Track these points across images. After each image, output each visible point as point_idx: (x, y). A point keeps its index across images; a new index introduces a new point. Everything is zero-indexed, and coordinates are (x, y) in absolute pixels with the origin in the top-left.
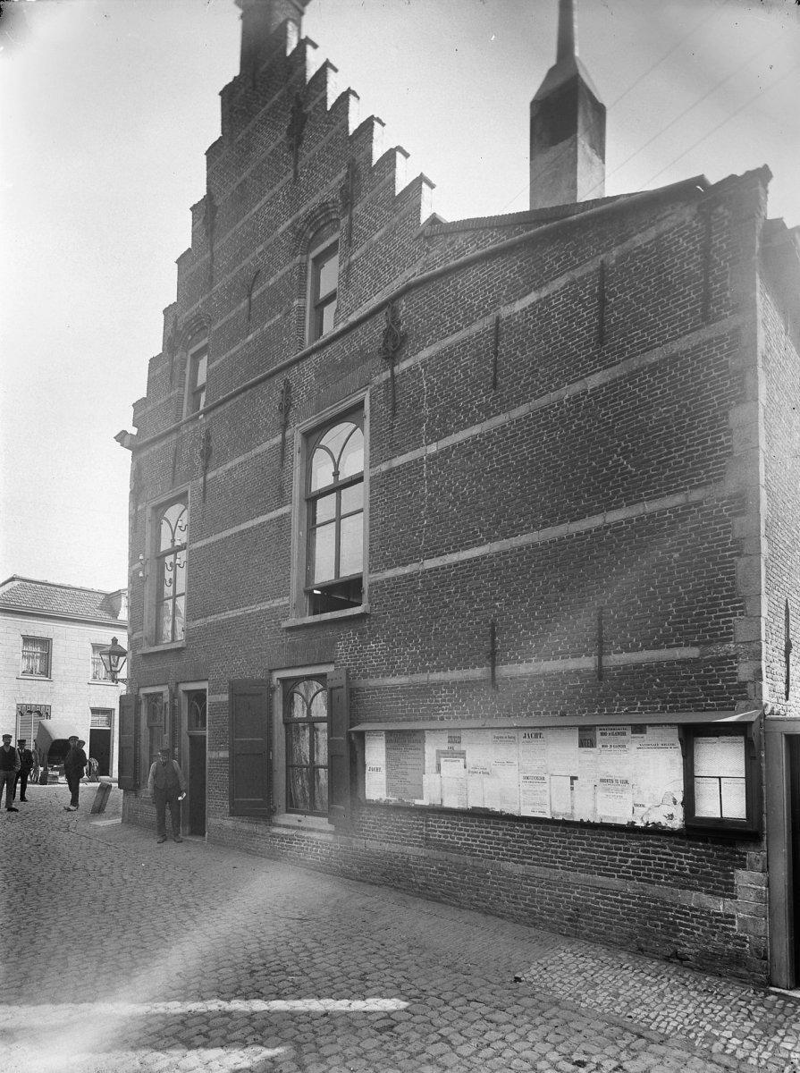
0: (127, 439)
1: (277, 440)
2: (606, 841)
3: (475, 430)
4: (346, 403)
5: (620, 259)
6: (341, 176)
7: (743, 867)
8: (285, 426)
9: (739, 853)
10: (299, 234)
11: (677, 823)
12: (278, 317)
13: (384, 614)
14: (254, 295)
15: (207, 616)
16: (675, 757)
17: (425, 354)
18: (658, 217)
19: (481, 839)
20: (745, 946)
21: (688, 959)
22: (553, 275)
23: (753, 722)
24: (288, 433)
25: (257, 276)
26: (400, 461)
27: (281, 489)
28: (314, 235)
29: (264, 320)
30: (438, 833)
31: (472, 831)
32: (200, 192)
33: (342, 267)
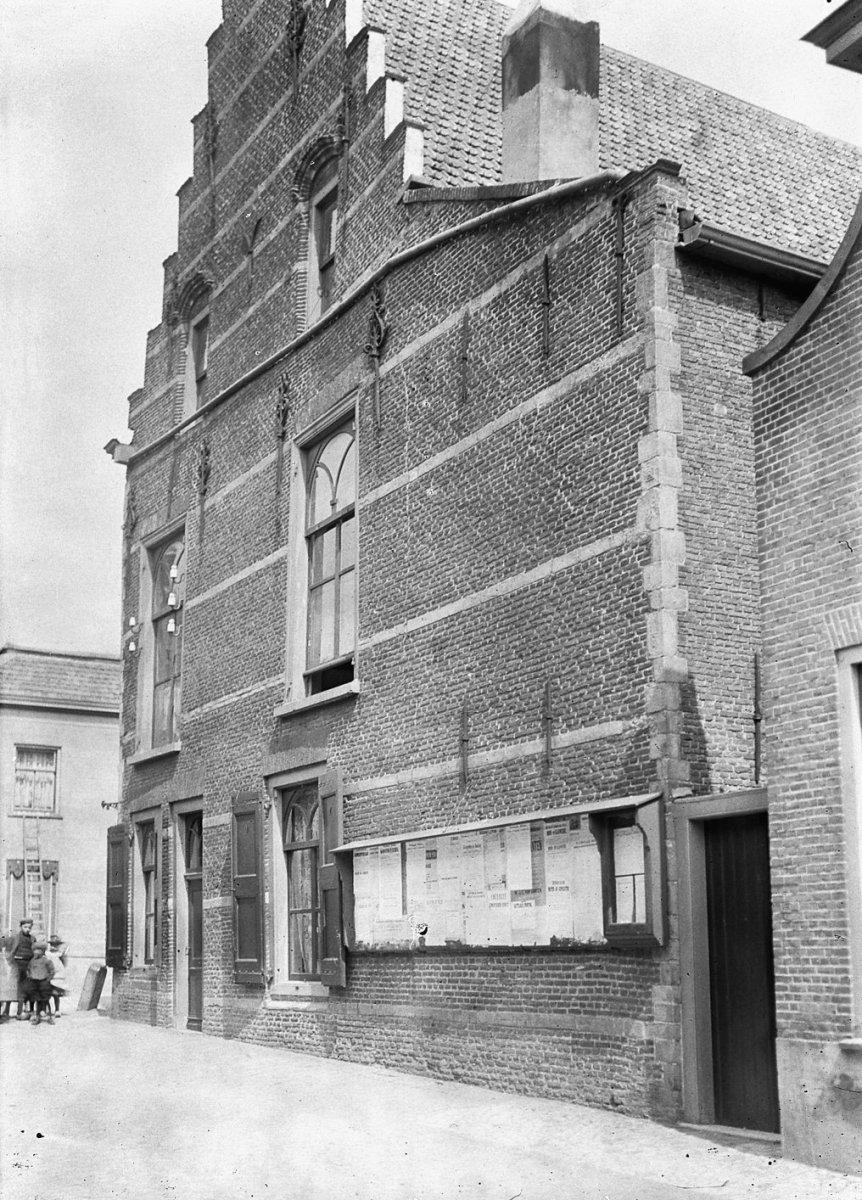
0: (118, 450)
1: (273, 456)
2: (558, 968)
3: (451, 452)
4: (338, 411)
5: (561, 254)
6: (339, 100)
7: (656, 981)
8: (283, 437)
9: (654, 965)
10: (300, 176)
11: (592, 931)
12: (278, 285)
13: (373, 692)
14: (257, 250)
15: (202, 705)
16: (592, 857)
17: (407, 352)
18: (587, 208)
19: (460, 984)
20: (660, 1077)
21: (622, 1104)
22: (509, 266)
23: (178, 752)
24: (286, 447)
25: (257, 229)
26: (385, 489)
27: (278, 524)
28: (316, 174)
29: (265, 289)
30: (423, 983)
31: (453, 975)
32: (201, 101)
33: (398, 155)
